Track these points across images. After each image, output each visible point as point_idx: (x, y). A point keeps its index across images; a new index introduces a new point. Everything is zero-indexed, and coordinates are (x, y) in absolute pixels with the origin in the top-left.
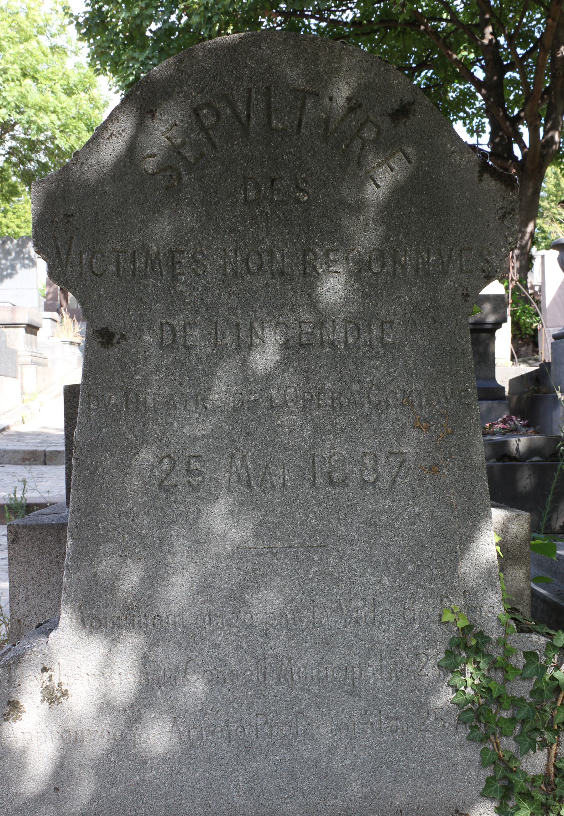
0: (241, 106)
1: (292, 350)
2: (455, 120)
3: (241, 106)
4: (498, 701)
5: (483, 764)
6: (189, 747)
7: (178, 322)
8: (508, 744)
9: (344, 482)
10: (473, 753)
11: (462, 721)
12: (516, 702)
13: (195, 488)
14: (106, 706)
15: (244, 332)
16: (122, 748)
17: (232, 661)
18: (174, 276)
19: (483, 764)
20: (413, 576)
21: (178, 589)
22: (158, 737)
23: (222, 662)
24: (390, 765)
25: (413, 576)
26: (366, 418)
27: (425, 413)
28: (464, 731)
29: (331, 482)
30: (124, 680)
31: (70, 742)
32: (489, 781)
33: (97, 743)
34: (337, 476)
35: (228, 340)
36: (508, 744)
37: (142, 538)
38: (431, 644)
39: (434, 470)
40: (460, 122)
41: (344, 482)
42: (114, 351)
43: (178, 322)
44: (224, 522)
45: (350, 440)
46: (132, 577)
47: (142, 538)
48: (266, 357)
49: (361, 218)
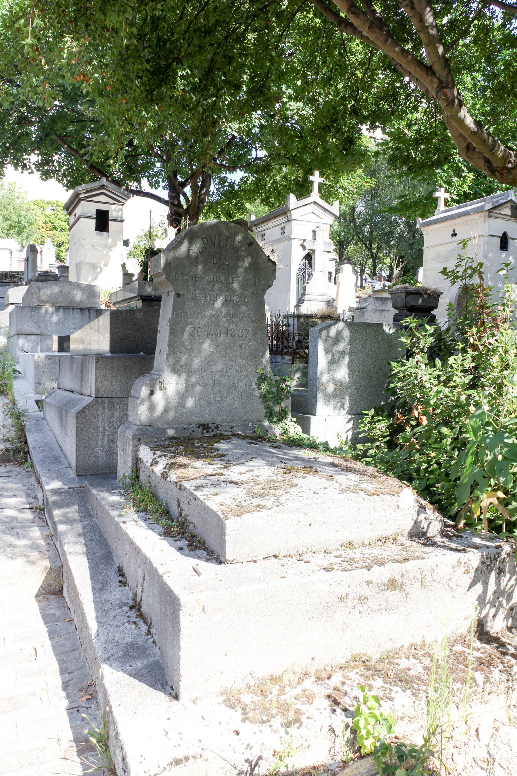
0: (213, 239)
1: (226, 303)
2: (143, 177)
3: (213, 239)
4: (269, 392)
5: (265, 408)
6: (196, 403)
7: (197, 292)
8: (271, 404)
9: (234, 336)
10: (262, 406)
11: (260, 397)
12: (273, 393)
13: (199, 336)
14: (178, 393)
15: (212, 297)
16: (181, 403)
17: (206, 381)
18: (196, 281)
19: (265, 408)
20: (250, 360)
21: (196, 363)
22: (190, 403)
23: (204, 381)
24: (243, 409)
25: (250, 360)
26: (240, 320)
27: (254, 319)
28: (261, 400)
29: (232, 336)
30: (182, 386)
31: (168, 401)
32: (266, 413)
33: (174, 402)
34: (233, 334)
35: (208, 298)
36: (271, 404)
37: (186, 348)
38: (254, 378)
39: (256, 334)
40: (145, 179)
41: (234, 336)
42: (180, 299)
43: (197, 292)
44: (207, 346)
45: (236, 325)
46: (184, 359)
47: (186, 348)
48: (218, 304)
49: (6, 86)
